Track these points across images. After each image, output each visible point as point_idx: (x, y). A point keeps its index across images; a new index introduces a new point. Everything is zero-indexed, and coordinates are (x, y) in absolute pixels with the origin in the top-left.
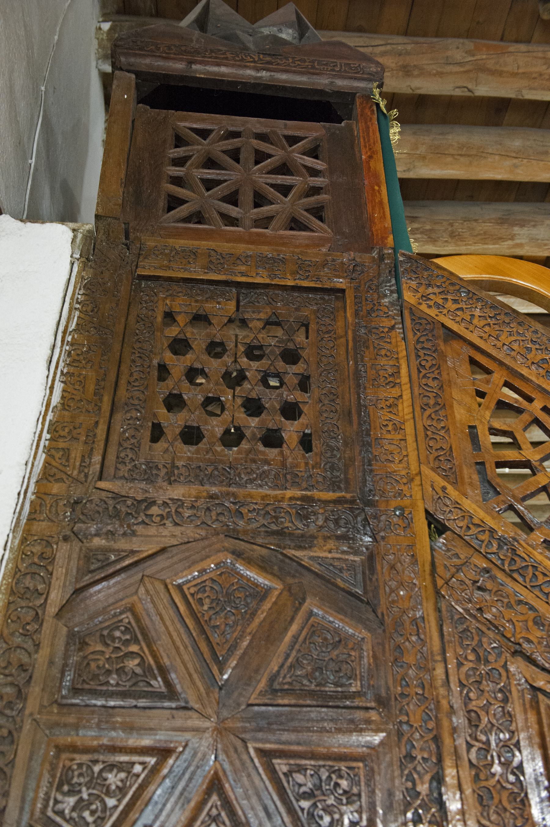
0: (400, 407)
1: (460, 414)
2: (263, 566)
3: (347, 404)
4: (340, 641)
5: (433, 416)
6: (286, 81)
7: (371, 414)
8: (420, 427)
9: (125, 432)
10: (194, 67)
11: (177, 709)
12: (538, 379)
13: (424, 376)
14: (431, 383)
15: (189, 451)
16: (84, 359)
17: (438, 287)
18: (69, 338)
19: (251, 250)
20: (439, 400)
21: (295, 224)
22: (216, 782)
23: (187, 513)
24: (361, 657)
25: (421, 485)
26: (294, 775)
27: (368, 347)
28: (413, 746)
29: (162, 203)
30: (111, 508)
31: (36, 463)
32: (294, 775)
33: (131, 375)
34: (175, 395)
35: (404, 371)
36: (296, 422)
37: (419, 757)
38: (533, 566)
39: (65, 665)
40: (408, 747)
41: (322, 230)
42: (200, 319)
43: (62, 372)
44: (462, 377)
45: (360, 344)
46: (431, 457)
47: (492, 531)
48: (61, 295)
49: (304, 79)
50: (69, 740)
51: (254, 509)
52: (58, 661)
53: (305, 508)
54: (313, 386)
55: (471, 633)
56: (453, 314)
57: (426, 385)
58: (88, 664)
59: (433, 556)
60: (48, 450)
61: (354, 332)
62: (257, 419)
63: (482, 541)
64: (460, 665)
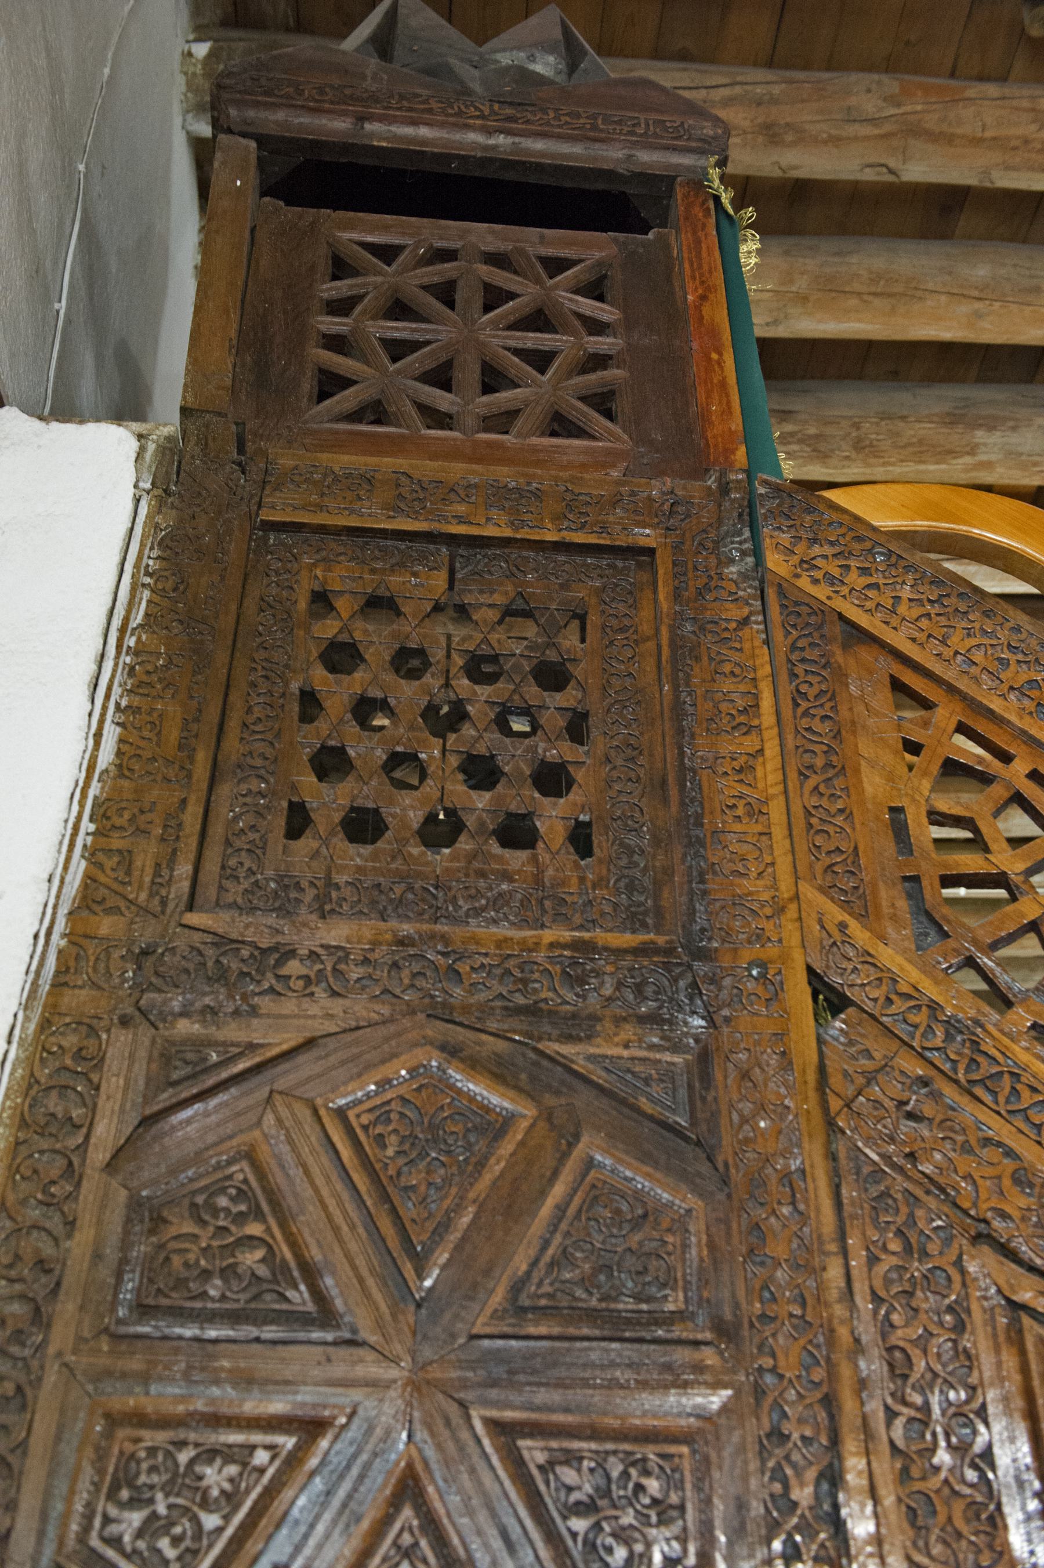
0: (760, 772)
1: (873, 784)
2: (499, 1072)
3: (659, 765)
4: (645, 1216)
5: (822, 788)
6: (542, 154)
7: (705, 785)
8: (797, 810)
9: (236, 818)
10: (368, 126)
11: (335, 1343)
12: (1021, 718)
13: (806, 713)
14: (817, 725)
15: (359, 855)
16: (160, 680)
17: (832, 544)
18: (132, 642)
19: (476, 473)
20: (834, 758)
21: (561, 425)
22: (411, 1483)
23: (355, 973)
24: (685, 1246)
25: (800, 919)
26: (559, 1469)
27: (698, 659)
28: (784, 1415)
29: (308, 385)
30: (210, 964)
31: (68, 878)
32: (559, 1469)
33: (249, 710)
34: (333, 749)
35: (767, 703)
36: (562, 801)
37: (796, 1436)
38: (1011, 1073)
39: (124, 1261)
40: (775, 1417)
41: (611, 436)
42: (379, 604)
43: (118, 705)
44: (877, 714)
45: (684, 652)
46: (819, 867)
47: (934, 1007)
48: (116, 559)
49: (577, 149)
50: (131, 1402)
51: (483, 965)
52: (111, 1253)
53: (579, 962)
54: (595, 733)
55: (895, 1200)
56: (860, 595)
57: (809, 729)
58: (167, 1259)
59: (821, 1055)
60: (91, 854)
61: (672, 629)
62: (488, 795)
63: (916, 1026)
64: (873, 1260)
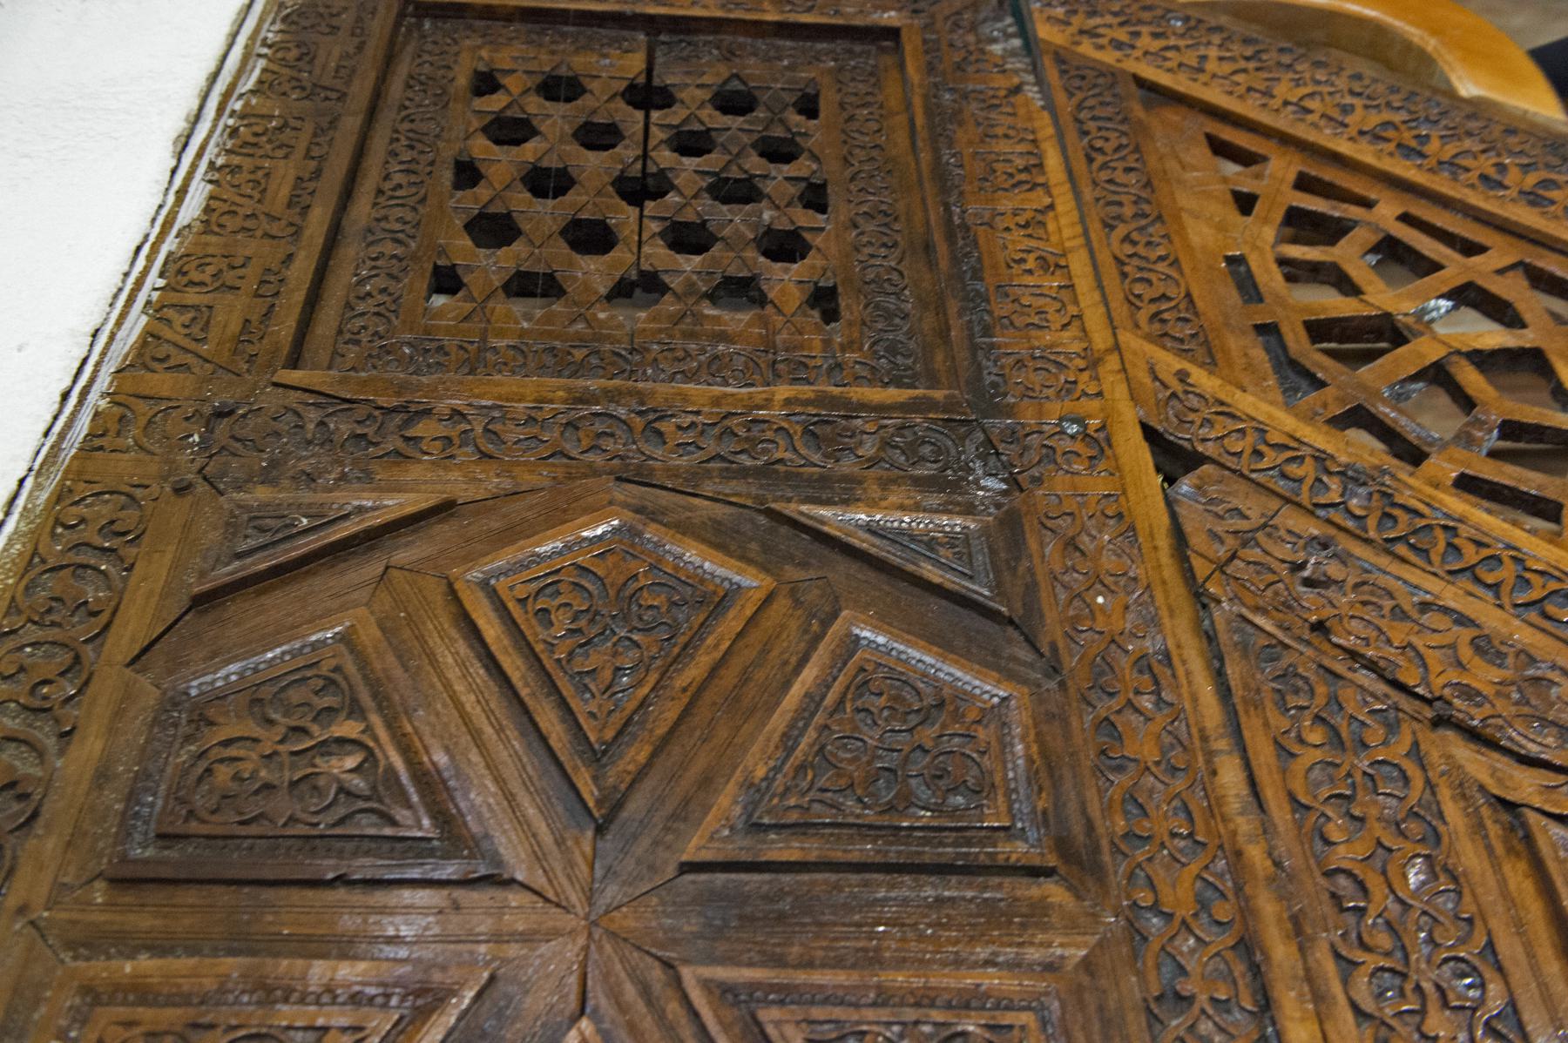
0: (1051, 227)
1: (1200, 234)
2: (720, 538)
7: (982, 241)
8: (1104, 257)
9: (361, 282)
12: (1379, 158)
13: (1104, 166)
14: (1120, 176)
16: (270, 141)
17: (1116, 14)
18: (238, 106)
20: (1146, 207)
23: (512, 434)
24: (1004, 745)
25: (1124, 370)
28: (1182, 970)
31: (120, 335)
35: (1053, 160)
36: (795, 266)
37: (1203, 999)
38: (1445, 527)
40: (1168, 969)
42: (559, 88)
43: (212, 164)
44: (1194, 168)
45: (941, 122)
46: (1143, 317)
47: (1321, 458)
48: (225, 29)
50: (128, 969)
51: (693, 424)
53: (827, 427)
55: (1306, 680)
56: (1158, 57)
57: (1110, 181)
59: (1174, 516)
60: (156, 310)
63: (1300, 480)
64: (1284, 753)
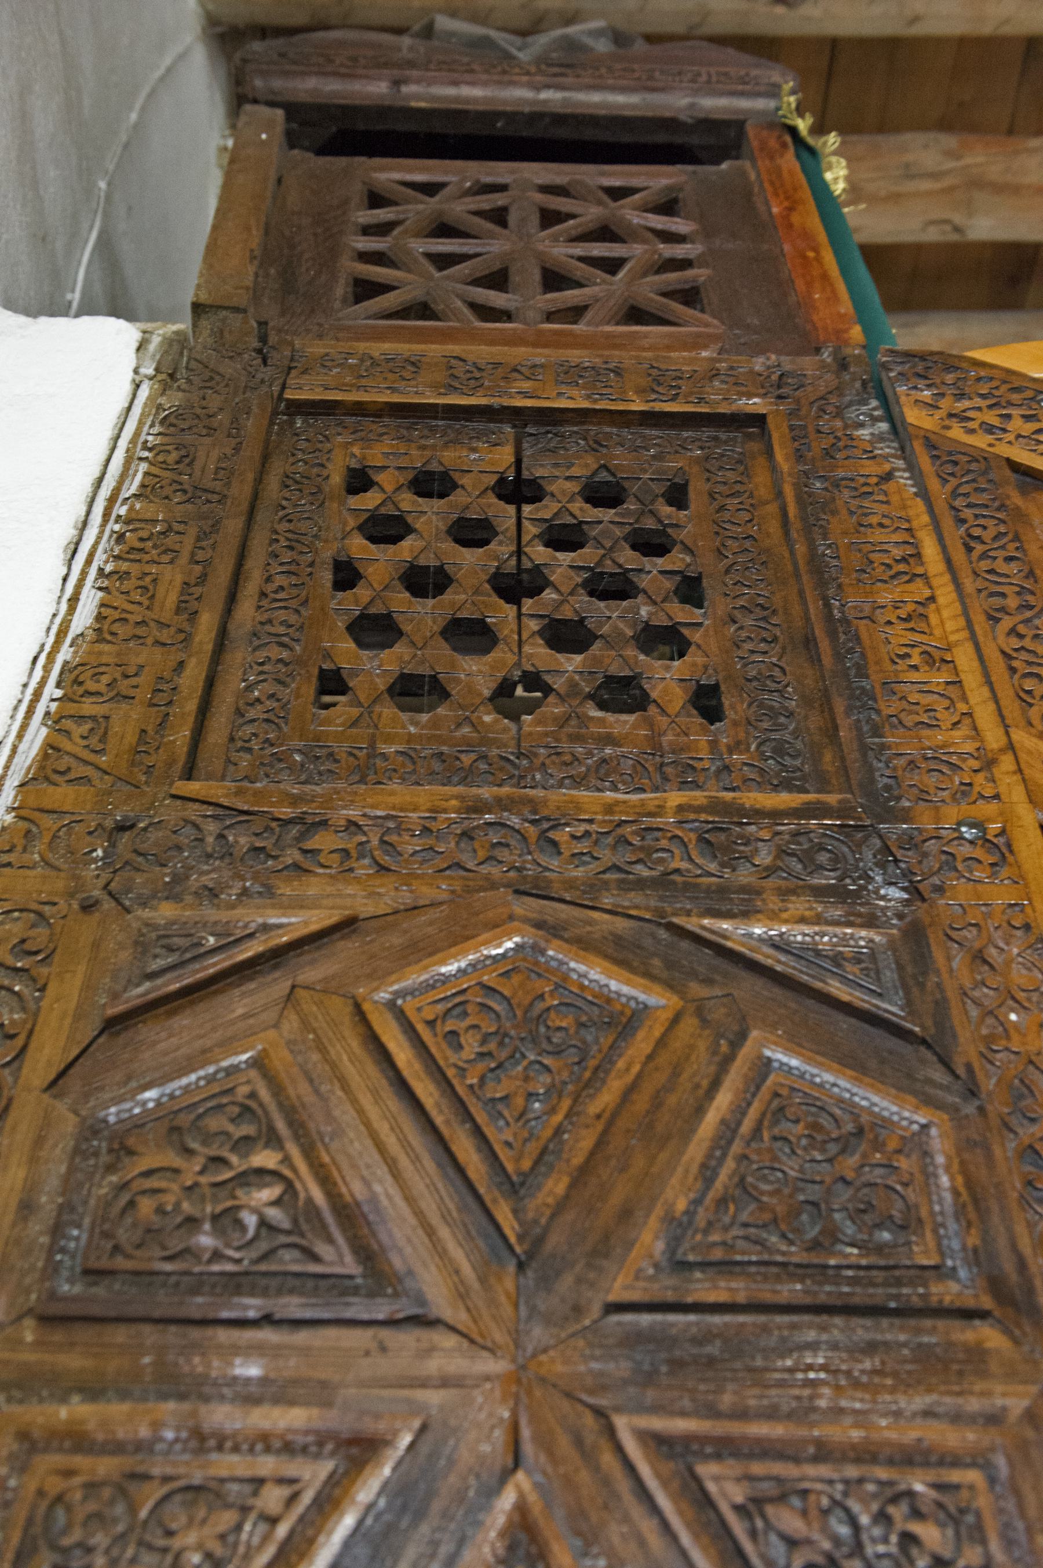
0: (934, 619)
2: (621, 954)
3: (799, 623)
4: (860, 1132)
5: (1021, 629)
6: (596, 105)
9: (249, 688)
10: (405, 89)
11: (391, 1323)
13: (984, 556)
14: (1001, 567)
15: (416, 724)
16: (155, 546)
17: (983, 396)
19: (540, 356)
21: (636, 315)
22: (523, 1537)
23: (410, 845)
24: (929, 1176)
26: (770, 1510)
27: (834, 512)
29: (341, 289)
30: (210, 840)
31: (22, 748)
32: (770, 1510)
33: (269, 579)
34: (377, 617)
35: (930, 549)
39: (67, 1207)
41: (697, 322)
42: (431, 484)
43: (101, 570)
45: (814, 513)
48: (108, 433)
49: (634, 99)
52: (47, 1201)
53: (721, 833)
54: (709, 593)
57: (991, 571)
58: (132, 1204)
60: (56, 721)
61: (796, 486)
62: (578, 658)
